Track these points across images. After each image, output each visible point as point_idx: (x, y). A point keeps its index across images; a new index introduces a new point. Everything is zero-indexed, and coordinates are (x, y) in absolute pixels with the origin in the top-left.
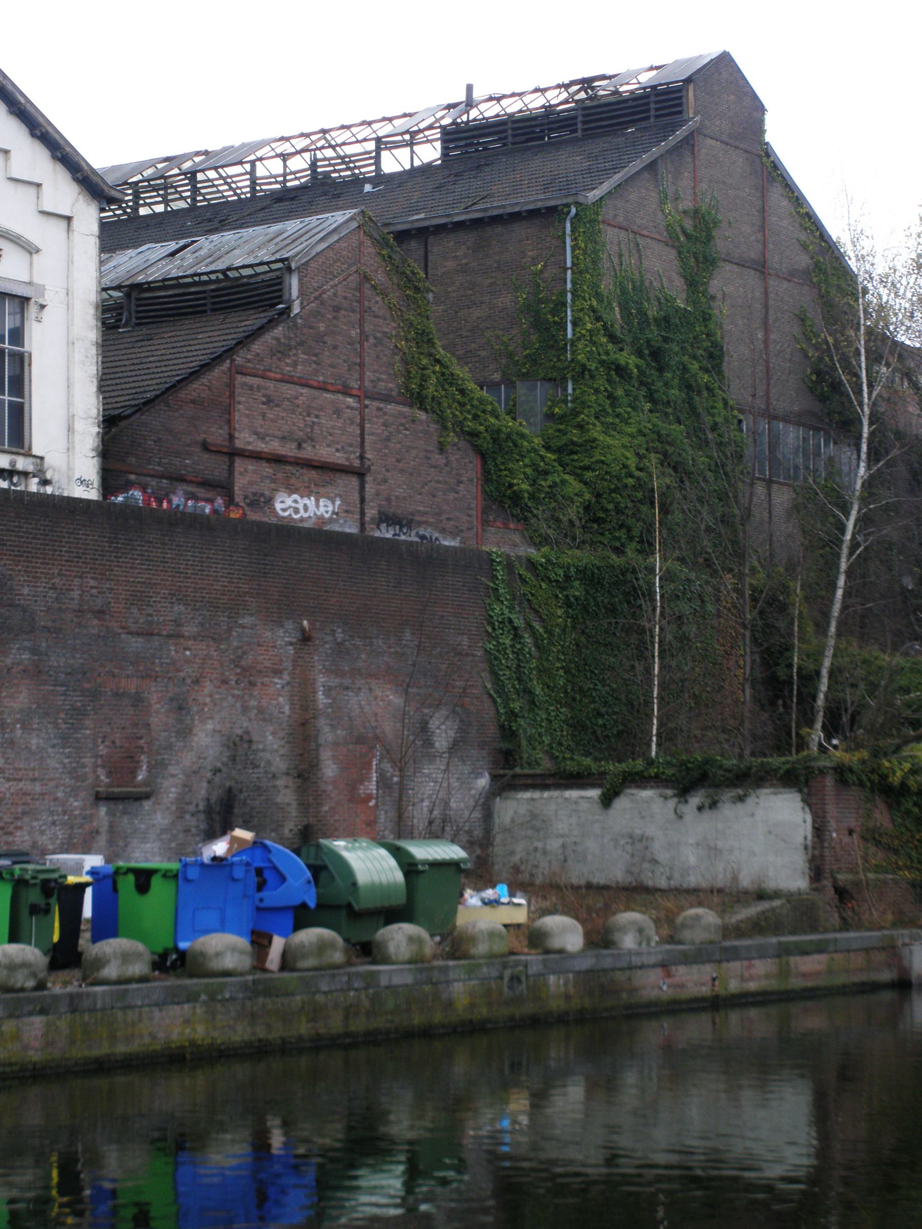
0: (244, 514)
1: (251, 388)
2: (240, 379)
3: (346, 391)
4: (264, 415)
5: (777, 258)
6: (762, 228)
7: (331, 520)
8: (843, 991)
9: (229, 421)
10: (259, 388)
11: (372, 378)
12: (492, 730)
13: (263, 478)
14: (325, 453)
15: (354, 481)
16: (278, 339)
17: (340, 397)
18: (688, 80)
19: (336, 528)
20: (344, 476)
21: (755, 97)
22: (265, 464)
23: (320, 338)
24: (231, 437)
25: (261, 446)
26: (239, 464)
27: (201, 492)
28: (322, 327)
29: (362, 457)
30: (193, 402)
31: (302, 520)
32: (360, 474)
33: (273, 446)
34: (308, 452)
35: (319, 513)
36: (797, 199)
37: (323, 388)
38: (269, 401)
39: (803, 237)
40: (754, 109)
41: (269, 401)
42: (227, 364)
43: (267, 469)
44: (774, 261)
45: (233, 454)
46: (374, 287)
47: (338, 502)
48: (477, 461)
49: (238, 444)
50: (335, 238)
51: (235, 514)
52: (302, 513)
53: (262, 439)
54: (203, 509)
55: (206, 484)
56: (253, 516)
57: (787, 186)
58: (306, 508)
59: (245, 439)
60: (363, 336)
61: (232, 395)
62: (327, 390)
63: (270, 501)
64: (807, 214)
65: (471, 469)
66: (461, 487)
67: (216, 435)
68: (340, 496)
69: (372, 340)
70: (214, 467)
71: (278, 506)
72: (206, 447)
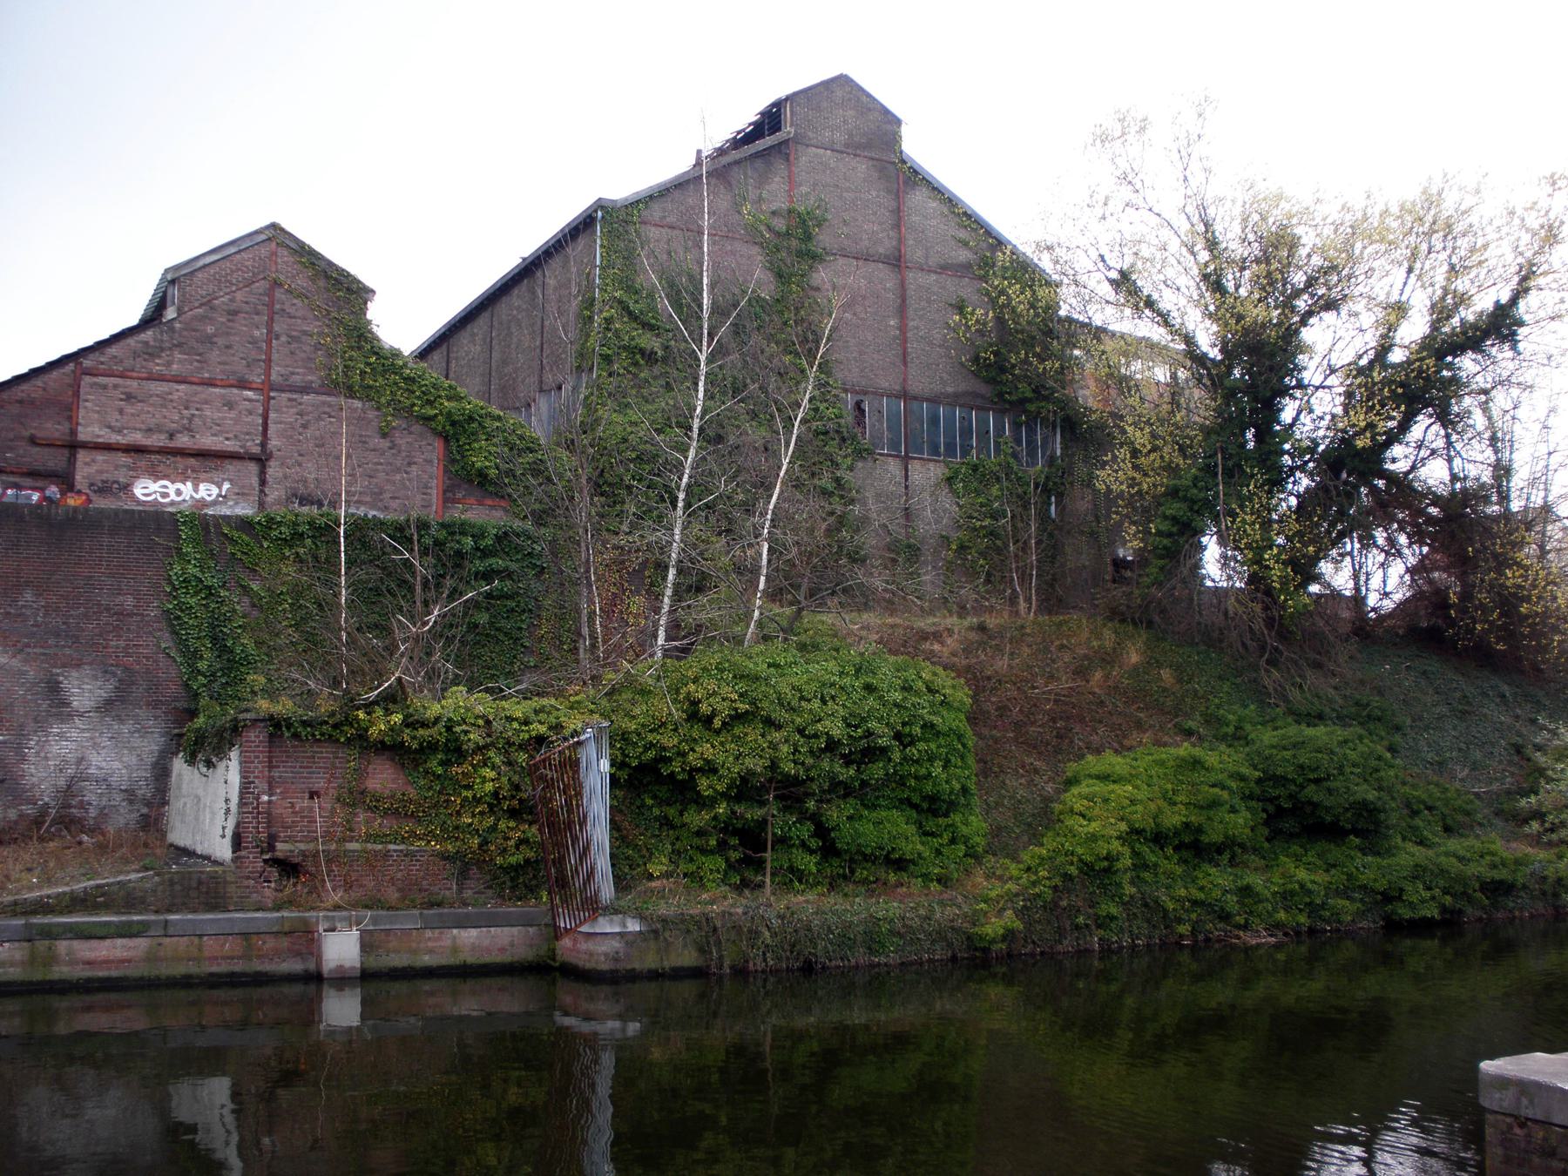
0: (89, 501)
1: (105, 387)
2: (87, 379)
3: (243, 384)
4: (121, 411)
5: (919, 253)
6: (897, 226)
7: (215, 503)
8: (214, 982)
9: (70, 418)
10: (116, 386)
11: (283, 371)
12: (174, 689)
13: (117, 467)
15: (253, 468)
16: (146, 343)
17: (235, 391)
18: (787, 98)
19: (225, 511)
20: (235, 462)
21: (886, 112)
22: (120, 454)
23: (209, 340)
24: (73, 432)
25: (115, 438)
26: (82, 456)
27: (28, 481)
28: (210, 330)
29: (263, 445)
30: (20, 402)
31: (173, 503)
32: (262, 460)
33: (138, 438)
34: (183, 441)
35: (197, 497)
36: (950, 201)
37: (211, 383)
38: (129, 397)
39: (963, 234)
41: (129, 397)
42: (72, 366)
43: (123, 459)
44: (914, 253)
45: (73, 446)
46: (289, 291)
47: (226, 486)
48: (438, 444)
50: (233, 250)
51: (73, 501)
52: (173, 497)
53: (119, 431)
54: (29, 497)
55: (33, 474)
56: (101, 503)
57: (935, 189)
58: (179, 493)
59: (84, 434)
60: (271, 335)
61: (77, 394)
62: (215, 386)
63: (126, 488)
64: (965, 213)
65: (433, 450)
66: (414, 468)
67: (54, 429)
68: (231, 481)
69: (284, 339)
70: (53, 460)
71: (138, 492)
72: (33, 441)
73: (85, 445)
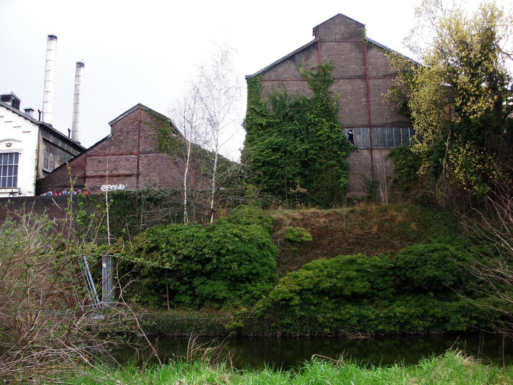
2: (88, 158)
3: (131, 153)
14: (121, 172)
24: (85, 174)
25: (95, 174)
32: (138, 176)
37: (122, 154)
38: (100, 162)
40: (359, 28)
41: (100, 162)
49: (87, 175)
73: (88, 177)
